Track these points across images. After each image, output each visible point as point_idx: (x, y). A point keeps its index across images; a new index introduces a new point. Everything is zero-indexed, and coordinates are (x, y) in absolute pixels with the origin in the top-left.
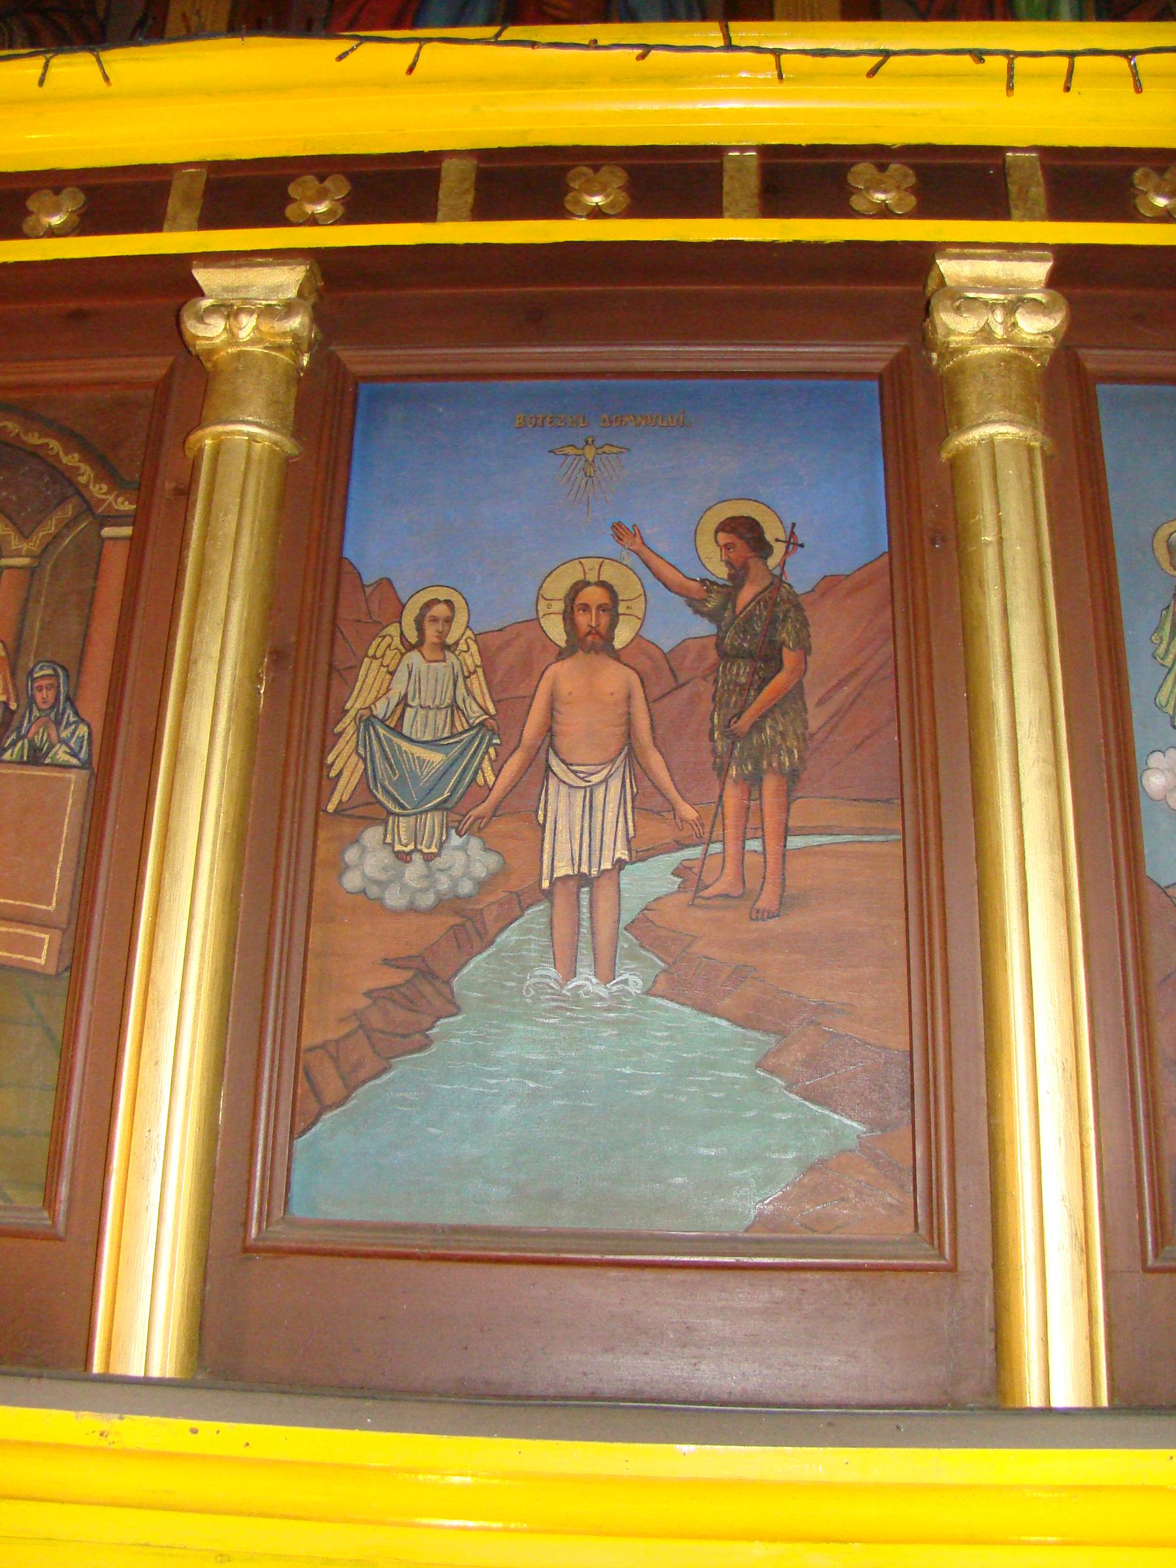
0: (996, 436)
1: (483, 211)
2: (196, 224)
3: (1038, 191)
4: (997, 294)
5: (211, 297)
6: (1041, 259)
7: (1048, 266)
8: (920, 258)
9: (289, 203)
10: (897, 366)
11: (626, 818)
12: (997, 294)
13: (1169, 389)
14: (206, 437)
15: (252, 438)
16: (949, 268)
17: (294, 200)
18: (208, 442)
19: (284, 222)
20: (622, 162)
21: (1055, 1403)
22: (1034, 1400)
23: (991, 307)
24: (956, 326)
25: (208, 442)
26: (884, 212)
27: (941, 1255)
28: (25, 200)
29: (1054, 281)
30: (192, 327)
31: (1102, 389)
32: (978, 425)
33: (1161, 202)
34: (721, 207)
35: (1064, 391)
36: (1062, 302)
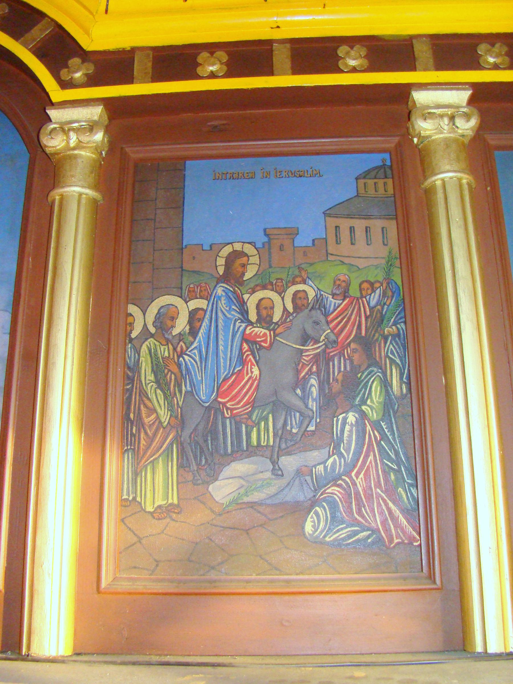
0: (449, 178)
1: (297, 70)
2: (150, 80)
3: (288, 64)
4: (442, 107)
5: (55, 123)
6: (464, 89)
7: (469, 93)
8: (403, 92)
9: (339, 60)
10: (399, 145)
11: (161, 351)
12: (442, 107)
13: (510, 153)
14: (56, 195)
15: (80, 194)
16: (420, 97)
17: (341, 58)
18: (57, 198)
19: (340, 71)
20: (226, 50)
21: (490, 650)
22: (479, 649)
23: (441, 116)
24: (424, 127)
25: (57, 198)
26: (213, 76)
27: (434, 582)
28: (196, 58)
29: (471, 101)
30: (45, 140)
31: (497, 154)
32: (439, 174)
33: (491, 60)
34: (133, 78)
35: (479, 154)
36: (476, 111)
